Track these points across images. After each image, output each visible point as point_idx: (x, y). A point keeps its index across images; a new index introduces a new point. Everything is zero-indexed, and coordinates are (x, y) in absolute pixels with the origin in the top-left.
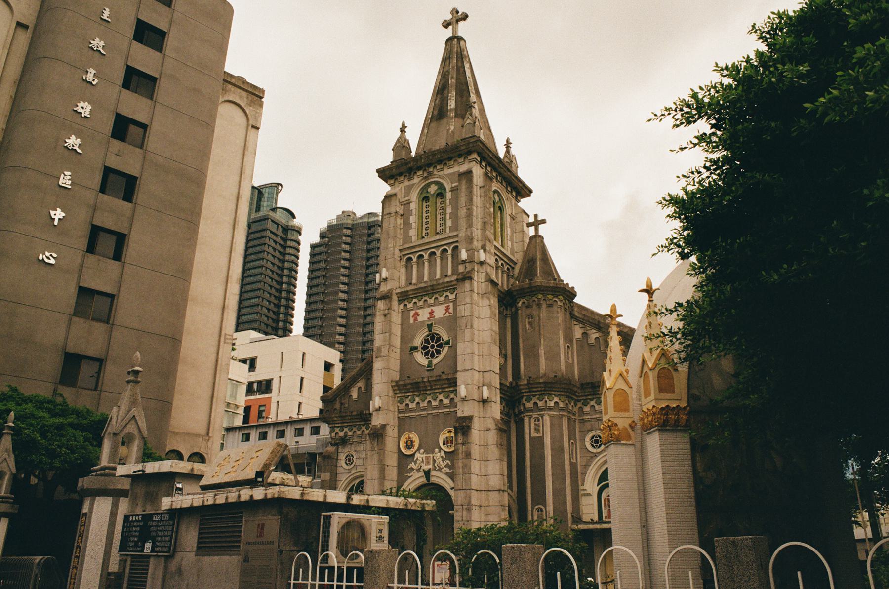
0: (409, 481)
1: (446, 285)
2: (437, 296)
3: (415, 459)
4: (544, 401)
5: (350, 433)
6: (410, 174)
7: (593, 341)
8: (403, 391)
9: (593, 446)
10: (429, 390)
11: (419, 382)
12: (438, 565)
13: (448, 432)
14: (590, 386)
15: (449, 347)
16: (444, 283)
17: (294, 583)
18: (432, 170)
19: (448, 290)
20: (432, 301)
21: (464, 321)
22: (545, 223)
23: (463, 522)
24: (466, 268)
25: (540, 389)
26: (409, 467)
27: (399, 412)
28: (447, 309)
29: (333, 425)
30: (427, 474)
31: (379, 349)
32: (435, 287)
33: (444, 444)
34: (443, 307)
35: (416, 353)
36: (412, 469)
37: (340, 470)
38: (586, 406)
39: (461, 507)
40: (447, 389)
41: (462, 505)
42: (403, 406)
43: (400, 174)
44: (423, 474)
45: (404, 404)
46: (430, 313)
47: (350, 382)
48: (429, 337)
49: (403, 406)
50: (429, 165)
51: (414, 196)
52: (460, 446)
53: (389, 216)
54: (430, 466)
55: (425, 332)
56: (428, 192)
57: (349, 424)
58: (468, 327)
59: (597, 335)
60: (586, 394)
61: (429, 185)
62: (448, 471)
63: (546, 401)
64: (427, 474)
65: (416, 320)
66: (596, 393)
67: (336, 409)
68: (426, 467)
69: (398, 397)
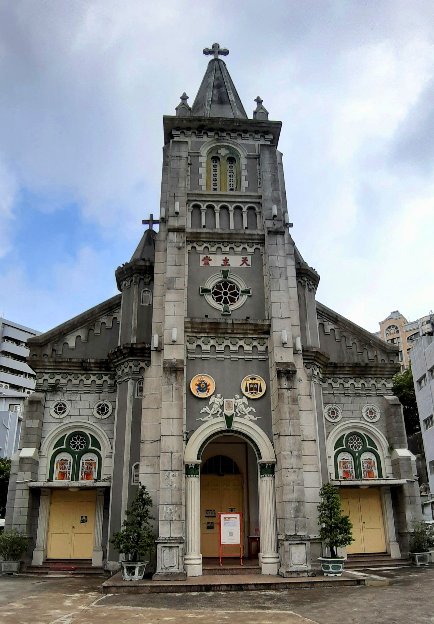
1: (246, 237)
2: (233, 246)
4: (311, 369)
5: (63, 381)
6: (200, 132)
8: (196, 330)
10: (230, 333)
11: (220, 323)
12: (225, 518)
13: (252, 379)
14: (333, 366)
16: (245, 234)
18: (225, 135)
19: (246, 242)
20: (227, 249)
21: (278, 271)
24: (274, 225)
25: (309, 358)
26: (202, 411)
28: (245, 260)
29: (42, 371)
30: (229, 420)
33: (246, 390)
35: (208, 296)
37: (47, 419)
40: (250, 336)
42: (193, 347)
43: (188, 129)
45: (195, 345)
46: (223, 260)
47: (68, 329)
48: (221, 284)
50: (223, 130)
51: (204, 151)
52: (285, 391)
53: (179, 158)
54: (233, 412)
55: (219, 278)
56: (218, 153)
57: (63, 371)
58: (282, 278)
59: (332, 327)
60: (327, 372)
61: (220, 147)
62: (253, 418)
63: (313, 370)
64: (229, 420)
65: (207, 264)
66: (335, 372)
67: (46, 355)
68: (229, 413)
69: (187, 336)
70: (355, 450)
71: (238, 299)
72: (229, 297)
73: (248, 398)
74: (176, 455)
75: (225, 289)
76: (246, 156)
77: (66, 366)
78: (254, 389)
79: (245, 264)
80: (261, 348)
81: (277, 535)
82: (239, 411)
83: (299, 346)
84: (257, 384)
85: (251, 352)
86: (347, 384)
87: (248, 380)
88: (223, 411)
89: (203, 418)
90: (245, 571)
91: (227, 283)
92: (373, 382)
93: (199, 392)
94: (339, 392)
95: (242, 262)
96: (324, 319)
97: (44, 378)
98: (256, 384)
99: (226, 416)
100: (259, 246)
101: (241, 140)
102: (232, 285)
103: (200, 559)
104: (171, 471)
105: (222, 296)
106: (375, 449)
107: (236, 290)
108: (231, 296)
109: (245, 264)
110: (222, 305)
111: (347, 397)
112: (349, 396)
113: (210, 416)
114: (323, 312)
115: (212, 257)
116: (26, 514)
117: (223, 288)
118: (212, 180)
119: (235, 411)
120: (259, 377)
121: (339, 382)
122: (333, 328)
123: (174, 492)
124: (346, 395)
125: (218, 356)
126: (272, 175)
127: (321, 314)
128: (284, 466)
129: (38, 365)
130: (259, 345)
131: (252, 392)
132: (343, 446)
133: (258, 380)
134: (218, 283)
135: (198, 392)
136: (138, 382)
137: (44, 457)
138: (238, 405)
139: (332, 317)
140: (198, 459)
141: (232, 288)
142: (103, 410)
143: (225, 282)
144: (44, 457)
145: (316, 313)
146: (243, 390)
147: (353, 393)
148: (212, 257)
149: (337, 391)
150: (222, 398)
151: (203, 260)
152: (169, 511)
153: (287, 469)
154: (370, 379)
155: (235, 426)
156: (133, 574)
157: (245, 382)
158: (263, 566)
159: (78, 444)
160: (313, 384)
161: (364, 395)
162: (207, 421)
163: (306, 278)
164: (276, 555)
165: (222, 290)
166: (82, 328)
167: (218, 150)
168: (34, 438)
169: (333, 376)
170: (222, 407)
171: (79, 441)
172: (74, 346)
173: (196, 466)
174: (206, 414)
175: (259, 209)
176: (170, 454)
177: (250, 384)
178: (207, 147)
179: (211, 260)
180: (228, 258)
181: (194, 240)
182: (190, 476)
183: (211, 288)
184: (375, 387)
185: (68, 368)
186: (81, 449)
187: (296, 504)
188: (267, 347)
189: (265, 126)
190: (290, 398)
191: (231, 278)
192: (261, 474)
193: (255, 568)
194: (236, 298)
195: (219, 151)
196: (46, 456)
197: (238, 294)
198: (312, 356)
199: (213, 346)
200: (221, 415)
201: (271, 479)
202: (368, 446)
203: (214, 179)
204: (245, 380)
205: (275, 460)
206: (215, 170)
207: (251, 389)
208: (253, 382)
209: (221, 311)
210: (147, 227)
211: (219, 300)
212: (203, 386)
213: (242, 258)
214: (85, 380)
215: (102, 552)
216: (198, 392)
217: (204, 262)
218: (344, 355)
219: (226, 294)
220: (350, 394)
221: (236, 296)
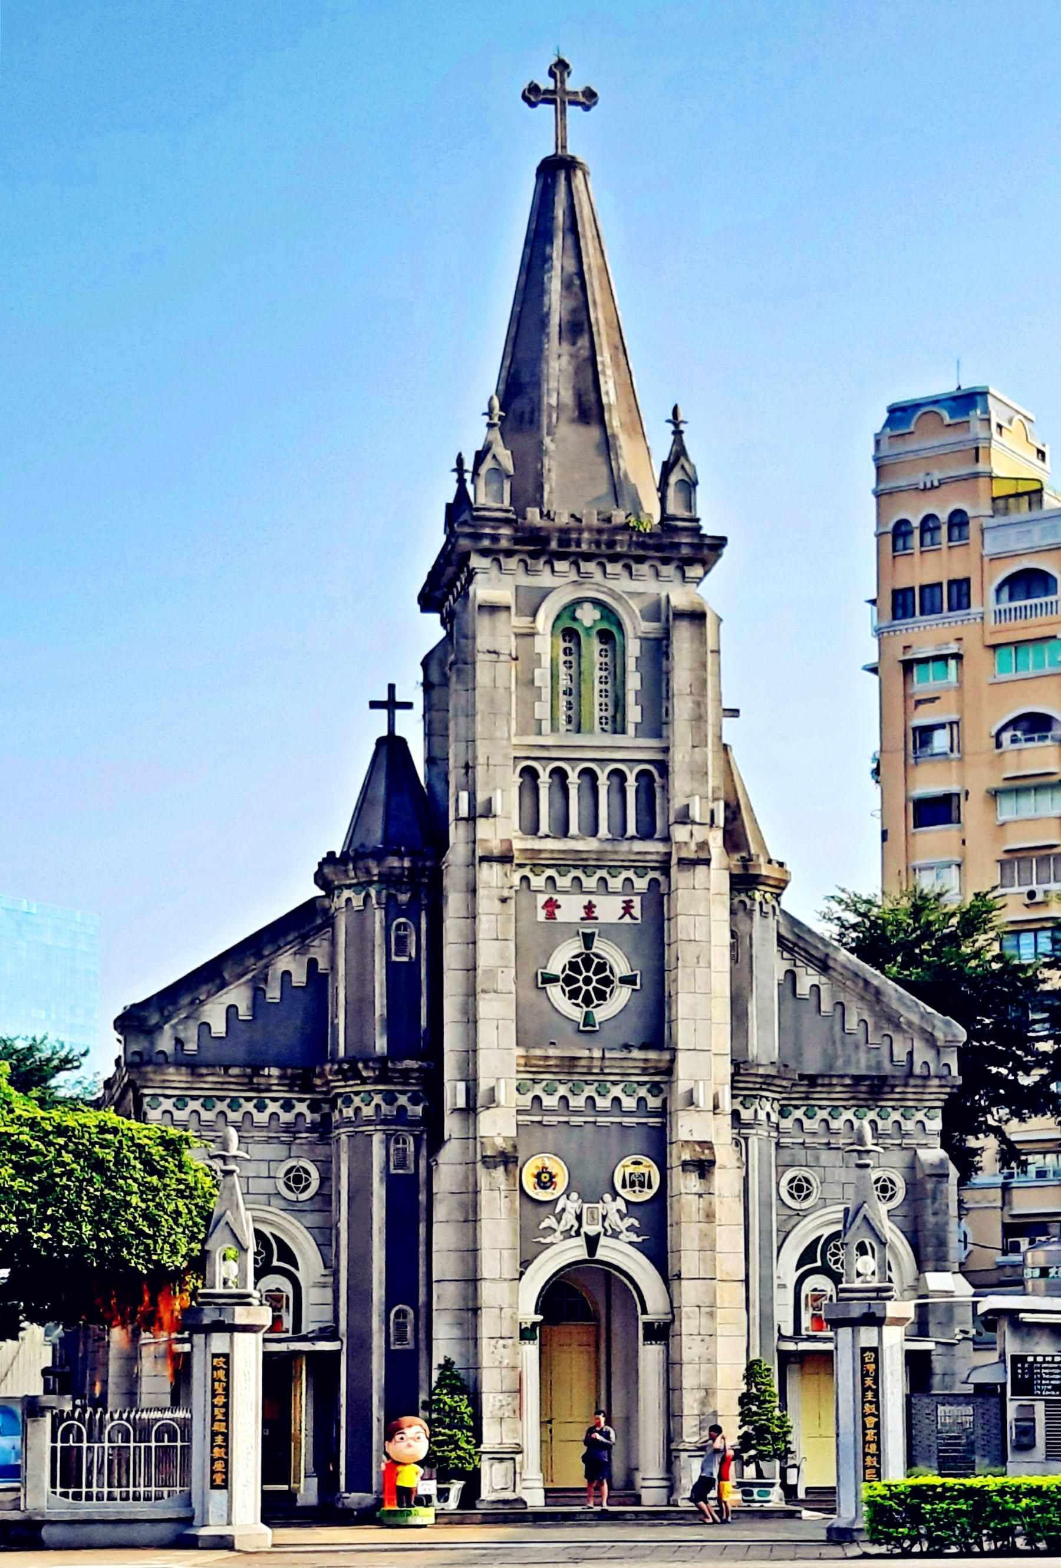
3: (558, 1209)
4: (752, 1110)
7: (807, 992)
9: (792, 1195)
13: (634, 1163)
15: (633, 990)
17: (62, 1447)
23: (700, 1337)
24: (692, 835)
26: (543, 1225)
27: (519, 1112)
28: (627, 908)
29: (159, 1091)
30: (592, 1243)
31: (490, 973)
32: (604, 856)
33: (624, 1186)
34: (618, 902)
35: (553, 989)
38: (786, 1117)
39: (697, 1309)
41: (699, 1306)
44: (584, 1243)
46: (585, 907)
48: (579, 960)
49: (526, 1100)
56: (575, 619)
58: (701, 964)
62: (634, 1238)
64: (592, 1243)
65: (551, 916)
68: (591, 1229)
73: (627, 1202)
74: (507, 1312)
77: (213, 1082)
79: (627, 916)
80: (653, 1103)
84: (643, 1174)
88: (580, 1226)
92: (896, 1116)
93: (539, 1190)
95: (622, 912)
109: (627, 916)
112: (838, 1149)
113: (558, 1234)
115: (560, 899)
119: (603, 1226)
120: (647, 1161)
121: (818, 1117)
122: (817, 983)
123: (504, 1371)
126: (694, 702)
129: (151, 1080)
130: (649, 1095)
140: (536, 1313)
141: (601, 968)
142: (298, 1179)
151: (543, 908)
152: (498, 1404)
154: (890, 1110)
155: (601, 1254)
156: (446, 1500)
158: (644, 1493)
162: (552, 1244)
166: (240, 985)
167: (574, 611)
169: (805, 1102)
170: (579, 1217)
173: (534, 1325)
174: (550, 1231)
175: (661, 776)
177: (631, 1174)
179: (559, 907)
180: (594, 902)
181: (527, 862)
185: (219, 1086)
187: (703, 1393)
190: (701, 1212)
191: (600, 946)
194: (608, 990)
197: (612, 982)
199: (563, 1098)
207: (632, 1184)
210: (378, 724)
213: (624, 902)
214: (254, 1111)
218: (836, 1049)
219: (587, 981)
221: (605, 970)
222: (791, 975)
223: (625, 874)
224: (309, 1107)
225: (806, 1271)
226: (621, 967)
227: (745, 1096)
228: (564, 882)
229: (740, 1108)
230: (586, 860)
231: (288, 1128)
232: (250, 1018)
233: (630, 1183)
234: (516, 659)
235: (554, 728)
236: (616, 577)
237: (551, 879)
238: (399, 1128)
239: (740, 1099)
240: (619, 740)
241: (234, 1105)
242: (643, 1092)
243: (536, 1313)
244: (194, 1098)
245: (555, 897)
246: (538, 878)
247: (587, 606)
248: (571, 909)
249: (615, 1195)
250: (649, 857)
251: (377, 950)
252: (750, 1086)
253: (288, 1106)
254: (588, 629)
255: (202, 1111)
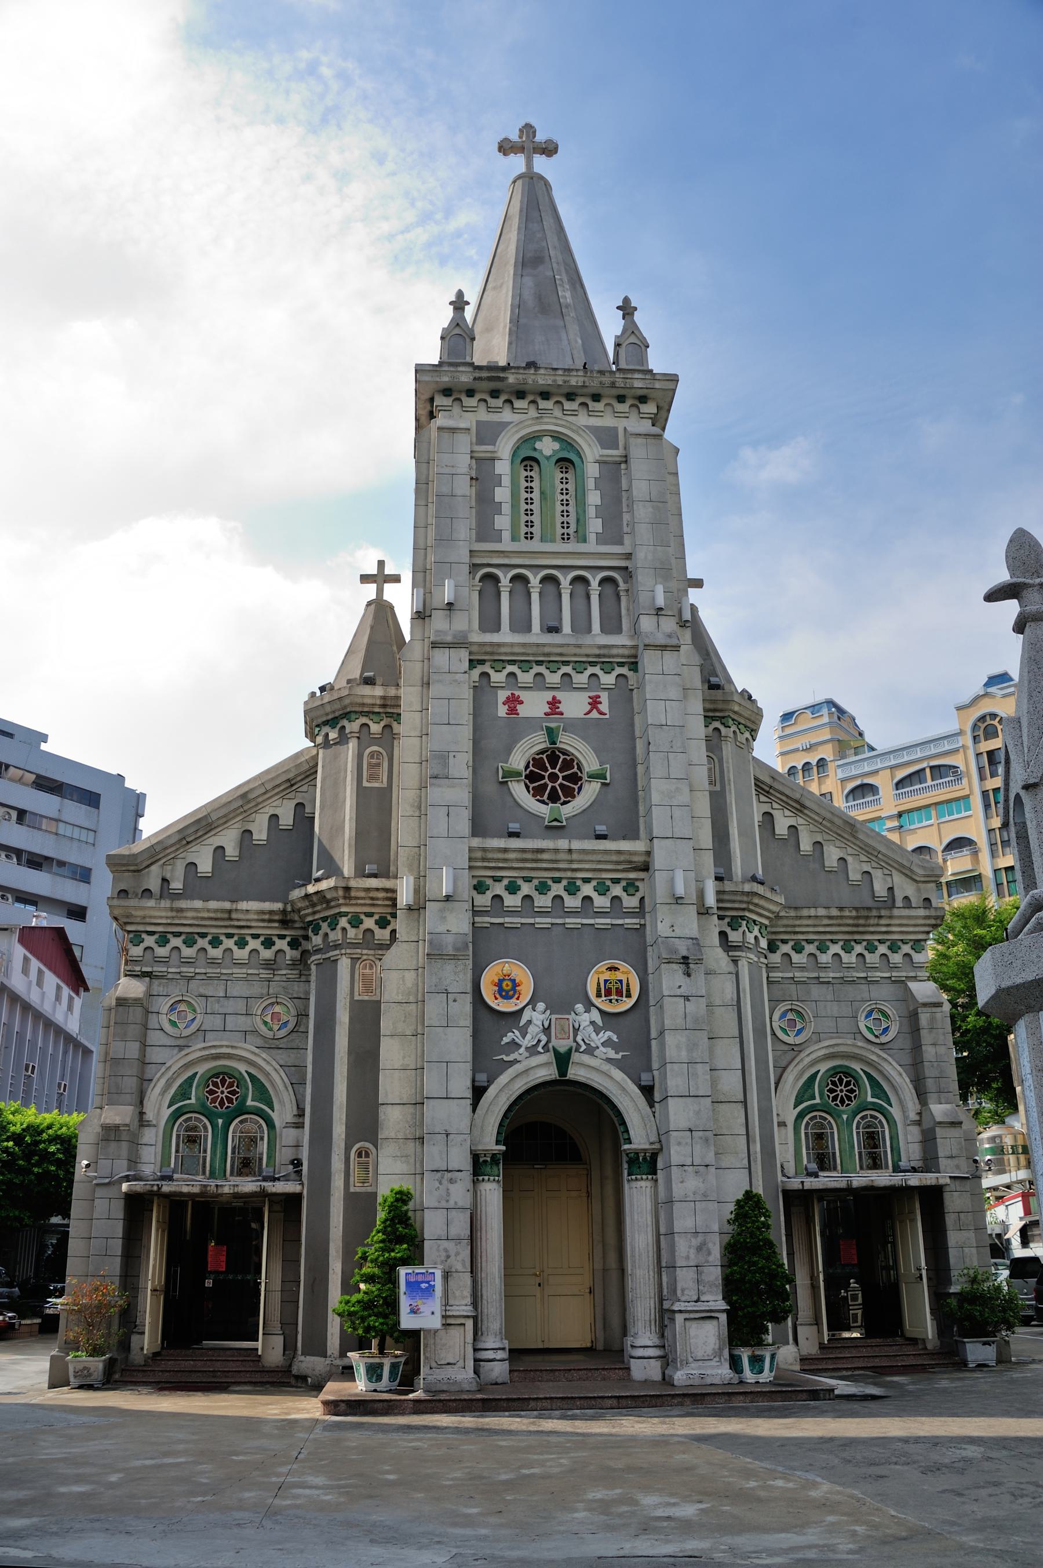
0: (511, 1072)
3: (522, 1022)
13: (611, 969)
22: (701, 587)
26: (506, 1040)
28: (595, 703)
30: (563, 1060)
33: (599, 995)
36: (515, 1045)
39: (689, 1133)
41: (691, 1131)
48: (544, 756)
49: (484, 900)
54: (570, 1042)
56: (535, 449)
62: (612, 1054)
63: (744, 932)
64: (563, 1060)
65: (513, 711)
70: (841, 1108)
71: (580, 789)
72: (561, 785)
75: (554, 767)
76: (598, 458)
78: (614, 991)
80: (630, 902)
81: (661, 1300)
82: (583, 1040)
83: (711, 900)
84: (621, 981)
85: (609, 910)
86: (824, 955)
87: (602, 972)
88: (549, 1041)
89: (507, 1055)
90: (596, 1374)
91: (557, 753)
93: (500, 1000)
94: (806, 974)
95: (589, 707)
96: (774, 803)
97: (146, 944)
98: (619, 980)
99: (556, 1053)
100: (624, 670)
101: (587, 416)
102: (568, 758)
103: (503, 1349)
104: (447, 1171)
105: (545, 783)
106: (885, 1105)
107: (575, 769)
108: (565, 783)
110: (547, 804)
111: (826, 986)
113: (522, 1050)
114: (771, 787)
115: (523, 695)
116: (119, 1253)
117: (548, 765)
118: (522, 512)
119: (575, 1041)
124: (821, 980)
125: (538, 920)
127: (768, 792)
128: (675, 1159)
130: (625, 894)
131: (609, 998)
132: (814, 1099)
133: (623, 972)
134: (538, 754)
135: (496, 999)
136: (359, 962)
137: (148, 1124)
138: (581, 1028)
139: (791, 798)
140: (498, 1143)
141: (568, 764)
143: (553, 752)
144: (148, 1124)
145: (753, 787)
146: (592, 993)
147: (838, 975)
148: (523, 695)
149: (802, 971)
150: (548, 1012)
153: (682, 1166)
157: (596, 977)
159: (224, 1096)
160: (746, 963)
161: (863, 981)
163: (730, 720)
164: (657, 1342)
165: (546, 770)
168: (130, 1084)
170: (547, 1030)
171: (226, 1091)
172: (210, 870)
175: (625, 582)
176: (445, 1136)
177: (606, 981)
178: (513, 435)
179: (522, 703)
182: (483, 1180)
183: (521, 767)
184: (889, 961)
186: (229, 1107)
188: (642, 899)
189: (640, 386)
192: (628, 1175)
193: (616, 1369)
195: (538, 445)
196: (154, 1122)
198: (741, 902)
199: (527, 897)
200: (546, 1048)
201: (649, 1184)
202: (870, 1099)
203: (527, 510)
204: (596, 972)
205: (657, 1146)
206: (529, 479)
207: (608, 993)
208: (613, 977)
209: (544, 818)
211: (538, 792)
212: (507, 985)
214: (235, 948)
215: (282, 1337)
216: (496, 999)
217: (507, 706)
219: (553, 777)
220: (831, 980)
222: (768, 816)
223: (591, 670)
224: (289, 944)
225: (807, 1107)
226: (589, 761)
227: (733, 917)
228: (526, 678)
229: (728, 930)
230: (548, 655)
231: (270, 965)
232: (237, 859)
233: (608, 991)
234: (477, 479)
235: (514, 538)
236: (574, 413)
237: (511, 674)
238: (365, 952)
239: (727, 920)
240: (581, 547)
241: (215, 942)
242: (617, 890)
243: (498, 1143)
244: (177, 935)
245: (517, 693)
246: (735, 933)
247: (547, 440)
248: (534, 705)
249: (589, 1005)
250: (615, 651)
251: (349, 778)
252: (736, 905)
253: (268, 943)
254: (548, 458)
255: (183, 947)
